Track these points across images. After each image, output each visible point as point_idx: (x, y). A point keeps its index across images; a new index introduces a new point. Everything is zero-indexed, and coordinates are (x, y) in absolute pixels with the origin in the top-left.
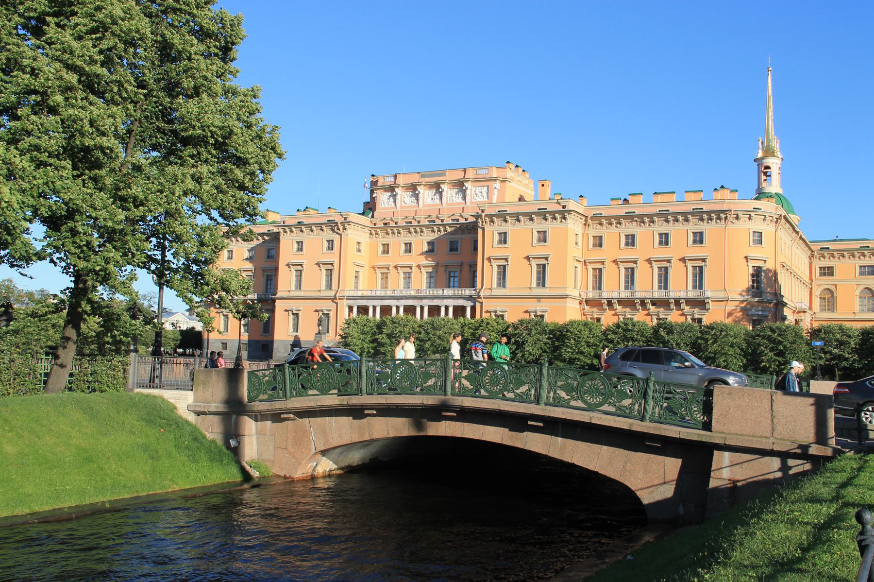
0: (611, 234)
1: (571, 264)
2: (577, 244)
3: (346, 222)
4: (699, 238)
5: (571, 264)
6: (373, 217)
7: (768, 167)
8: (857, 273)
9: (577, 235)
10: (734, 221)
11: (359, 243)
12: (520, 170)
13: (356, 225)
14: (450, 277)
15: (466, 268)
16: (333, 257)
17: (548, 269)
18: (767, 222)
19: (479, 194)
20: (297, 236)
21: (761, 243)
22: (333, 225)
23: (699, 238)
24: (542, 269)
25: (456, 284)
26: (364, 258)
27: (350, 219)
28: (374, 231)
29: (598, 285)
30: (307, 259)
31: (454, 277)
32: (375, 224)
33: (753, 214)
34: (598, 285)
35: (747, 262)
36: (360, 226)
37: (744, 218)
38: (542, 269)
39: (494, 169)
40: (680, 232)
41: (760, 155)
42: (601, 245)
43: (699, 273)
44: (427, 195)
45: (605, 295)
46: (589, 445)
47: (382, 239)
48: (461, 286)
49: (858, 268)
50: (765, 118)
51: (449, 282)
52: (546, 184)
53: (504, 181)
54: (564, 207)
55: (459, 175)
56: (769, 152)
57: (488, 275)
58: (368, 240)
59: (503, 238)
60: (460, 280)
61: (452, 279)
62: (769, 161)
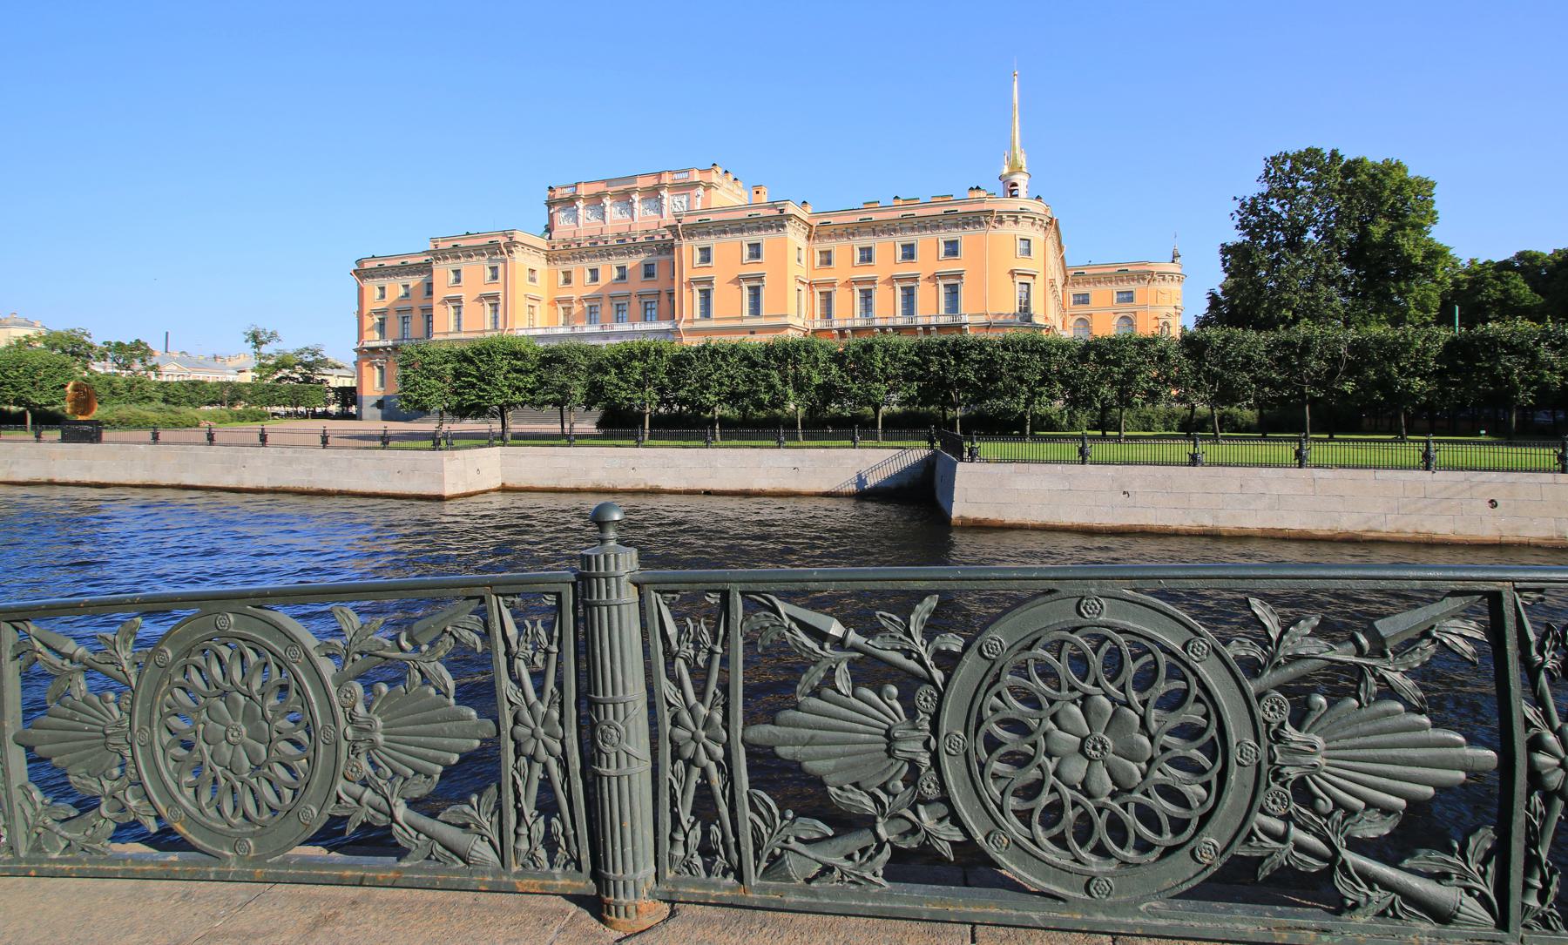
0: (841, 249)
1: (792, 285)
2: (799, 260)
3: (511, 245)
4: (952, 248)
5: (792, 285)
6: (550, 238)
7: (1015, 185)
8: (1115, 301)
9: (799, 249)
10: (997, 225)
11: (533, 271)
12: (731, 178)
13: (526, 248)
14: (646, 310)
15: (664, 298)
16: (496, 289)
17: (764, 293)
18: (1037, 227)
19: (679, 204)
20: (452, 264)
21: (1029, 254)
22: (493, 249)
23: (952, 248)
24: (755, 293)
25: (654, 318)
26: (541, 289)
27: (518, 237)
28: (551, 258)
29: (827, 313)
30: (467, 293)
31: (651, 309)
32: (553, 247)
33: (1020, 216)
34: (827, 313)
35: (1013, 277)
36: (531, 250)
37: (1009, 223)
38: (755, 293)
39: (696, 171)
40: (929, 245)
41: (1006, 170)
42: (829, 262)
43: (953, 291)
44: (612, 210)
45: (836, 324)
46: (933, 889)
47: (562, 267)
48: (659, 319)
49: (1115, 294)
50: (1010, 129)
51: (646, 316)
52: (762, 191)
53: (709, 186)
54: (781, 211)
55: (652, 182)
56: (1016, 168)
57: (690, 303)
58: (546, 267)
59: (706, 253)
60: (658, 312)
61: (649, 313)
62: (1017, 178)
